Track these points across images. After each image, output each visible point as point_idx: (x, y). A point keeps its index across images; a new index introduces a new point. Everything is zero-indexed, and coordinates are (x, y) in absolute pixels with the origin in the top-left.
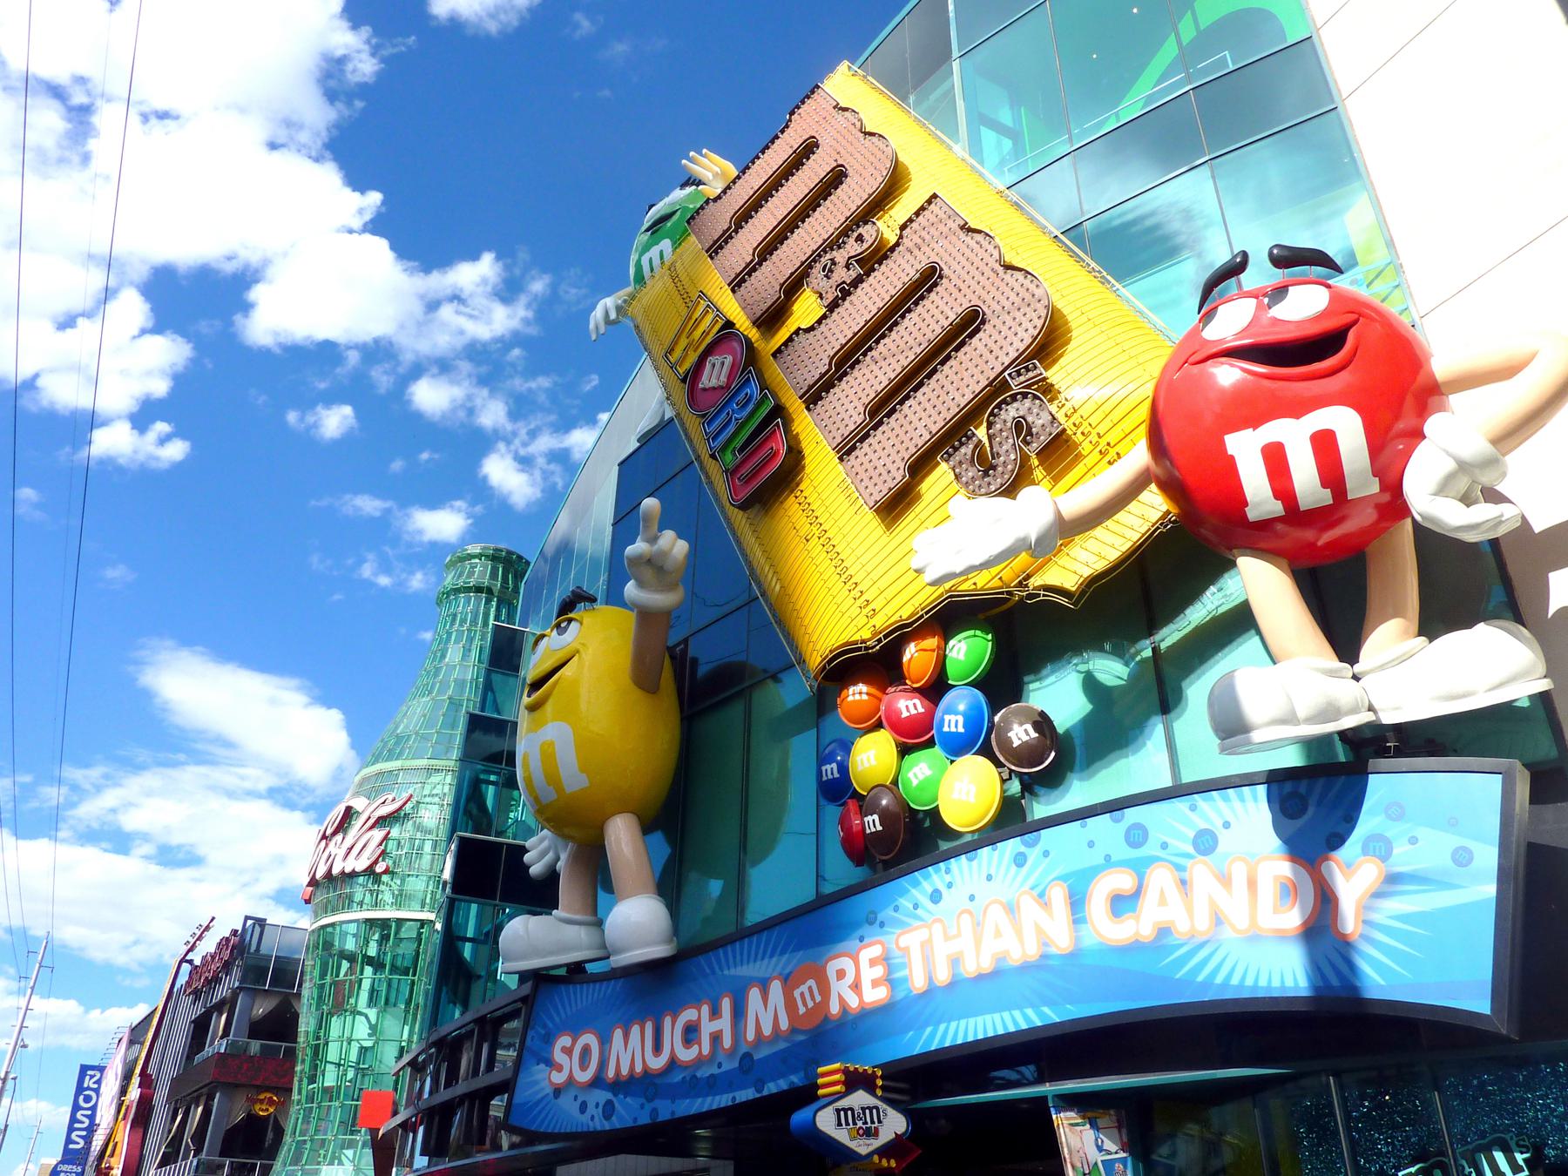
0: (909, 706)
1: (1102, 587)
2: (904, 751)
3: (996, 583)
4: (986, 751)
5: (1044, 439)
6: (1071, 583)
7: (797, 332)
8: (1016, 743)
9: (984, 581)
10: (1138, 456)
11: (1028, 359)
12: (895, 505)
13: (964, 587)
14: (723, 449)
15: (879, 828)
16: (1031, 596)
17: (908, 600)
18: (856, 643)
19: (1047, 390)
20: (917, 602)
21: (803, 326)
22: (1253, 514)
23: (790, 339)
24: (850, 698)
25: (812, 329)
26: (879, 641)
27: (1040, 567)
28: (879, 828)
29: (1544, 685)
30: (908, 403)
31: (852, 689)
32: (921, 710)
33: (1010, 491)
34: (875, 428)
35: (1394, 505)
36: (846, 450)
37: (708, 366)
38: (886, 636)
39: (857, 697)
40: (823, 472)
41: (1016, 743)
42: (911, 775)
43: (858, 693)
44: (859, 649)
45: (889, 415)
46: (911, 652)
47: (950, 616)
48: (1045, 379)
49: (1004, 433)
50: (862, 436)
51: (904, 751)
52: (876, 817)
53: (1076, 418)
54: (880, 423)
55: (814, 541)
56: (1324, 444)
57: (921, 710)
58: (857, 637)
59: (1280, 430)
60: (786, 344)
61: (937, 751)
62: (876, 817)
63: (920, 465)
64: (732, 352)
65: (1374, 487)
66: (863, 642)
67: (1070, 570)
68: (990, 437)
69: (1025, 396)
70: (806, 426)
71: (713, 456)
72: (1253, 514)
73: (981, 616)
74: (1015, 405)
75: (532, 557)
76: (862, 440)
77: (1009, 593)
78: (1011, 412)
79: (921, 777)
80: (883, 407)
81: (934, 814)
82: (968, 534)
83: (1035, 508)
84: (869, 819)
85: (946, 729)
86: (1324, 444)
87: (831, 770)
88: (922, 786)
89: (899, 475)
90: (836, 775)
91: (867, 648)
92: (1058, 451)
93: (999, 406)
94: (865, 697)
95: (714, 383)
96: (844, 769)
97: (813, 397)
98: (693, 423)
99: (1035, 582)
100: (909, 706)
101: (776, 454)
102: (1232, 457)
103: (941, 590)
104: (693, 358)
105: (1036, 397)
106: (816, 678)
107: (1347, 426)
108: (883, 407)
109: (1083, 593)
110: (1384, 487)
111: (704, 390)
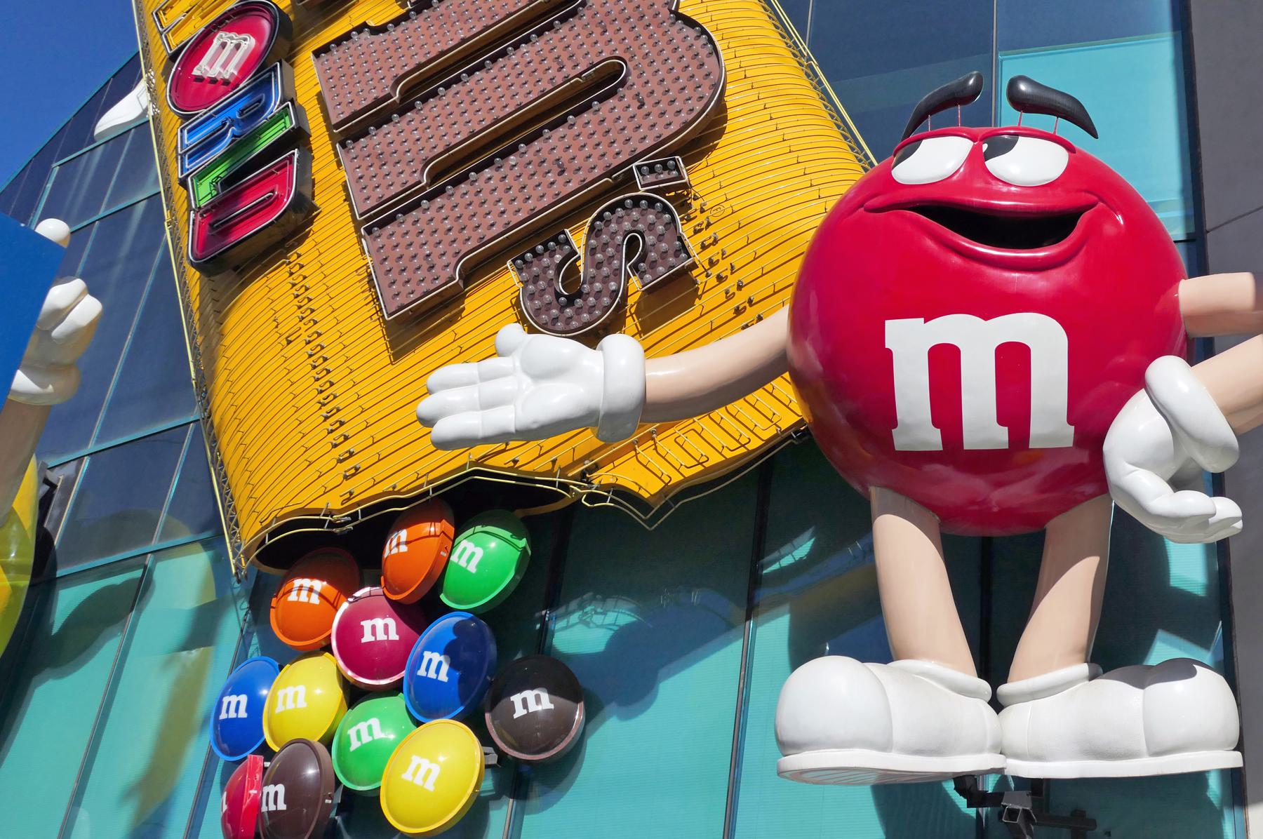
0: (381, 629)
1: (700, 500)
2: (354, 695)
3: (542, 465)
4: (474, 721)
5: (662, 272)
6: (649, 487)
7: (361, 28)
8: (367, 638)
9: (529, 459)
10: (774, 328)
11: (671, 152)
12: (417, 322)
13: (500, 461)
14: (201, 175)
15: (282, 806)
16: (592, 498)
17: (411, 469)
18: (316, 512)
19: (682, 199)
20: (422, 467)
21: (372, 24)
22: (902, 440)
23: (347, 37)
24: (293, 597)
25: (382, 29)
26: (354, 516)
27: (611, 459)
28: (282, 806)
29: (1234, 760)
30: (487, 172)
31: (298, 582)
32: (394, 636)
33: (591, 339)
34: (431, 197)
35: (1085, 470)
36: (375, 221)
37: (216, 43)
38: (365, 512)
39: (304, 597)
40: (333, 249)
41: (367, 638)
42: (352, 732)
43: (306, 591)
44: (320, 523)
45: (456, 183)
46: (397, 544)
47: (470, 498)
48: (686, 186)
49: (609, 248)
50: (408, 202)
51: (354, 695)
52: (281, 788)
53: (712, 252)
54: (440, 191)
55: (298, 344)
56: (1013, 362)
57: (394, 636)
58: (320, 504)
59: (955, 328)
60: (338, 41)
61: (398, 703)
62: (281, 788)
63: (478, 268)
64: (256, 33)
65: (1066, 435)
66: (330, 513)
67: (649, 470)
68: (592, 251)
69: (652, 202)
70: (327, 168)
71: (183, 183)
72: (902, 440)
73: (520, 513)
74: (635, 214)
75: (512, 332)
76: (405, 211)
77: (564, 486)
78: (624, 222)
79: (366, 739)
80: (452, 169)
81: (373, 799)
82: (515, 384)
83: (619, 367)
84: (271, 789)
85: (422, 672)
86: (1013, 362)
87: (236, 707)
88: (366, 752)
89: (448, 272)
90: (243, 714)
91: (332, 525)
92: (672, 294)
93: (611, 209)
94: (315, 599)
95: (212, 73)
96: (256, 707)
97: (350, 133)
98: (172, 121)
99: (604, 477)
100: (381, 629)
101: (278, 201)
102: (889, 352)
103: (463, 460)
104: (196, 26)
105: (666, 209)
106: (247, 553)
107: (1046, 340)
108: (452, 169)
109: (665, 508)
110: (1080, 440)
111: (200, 79)
